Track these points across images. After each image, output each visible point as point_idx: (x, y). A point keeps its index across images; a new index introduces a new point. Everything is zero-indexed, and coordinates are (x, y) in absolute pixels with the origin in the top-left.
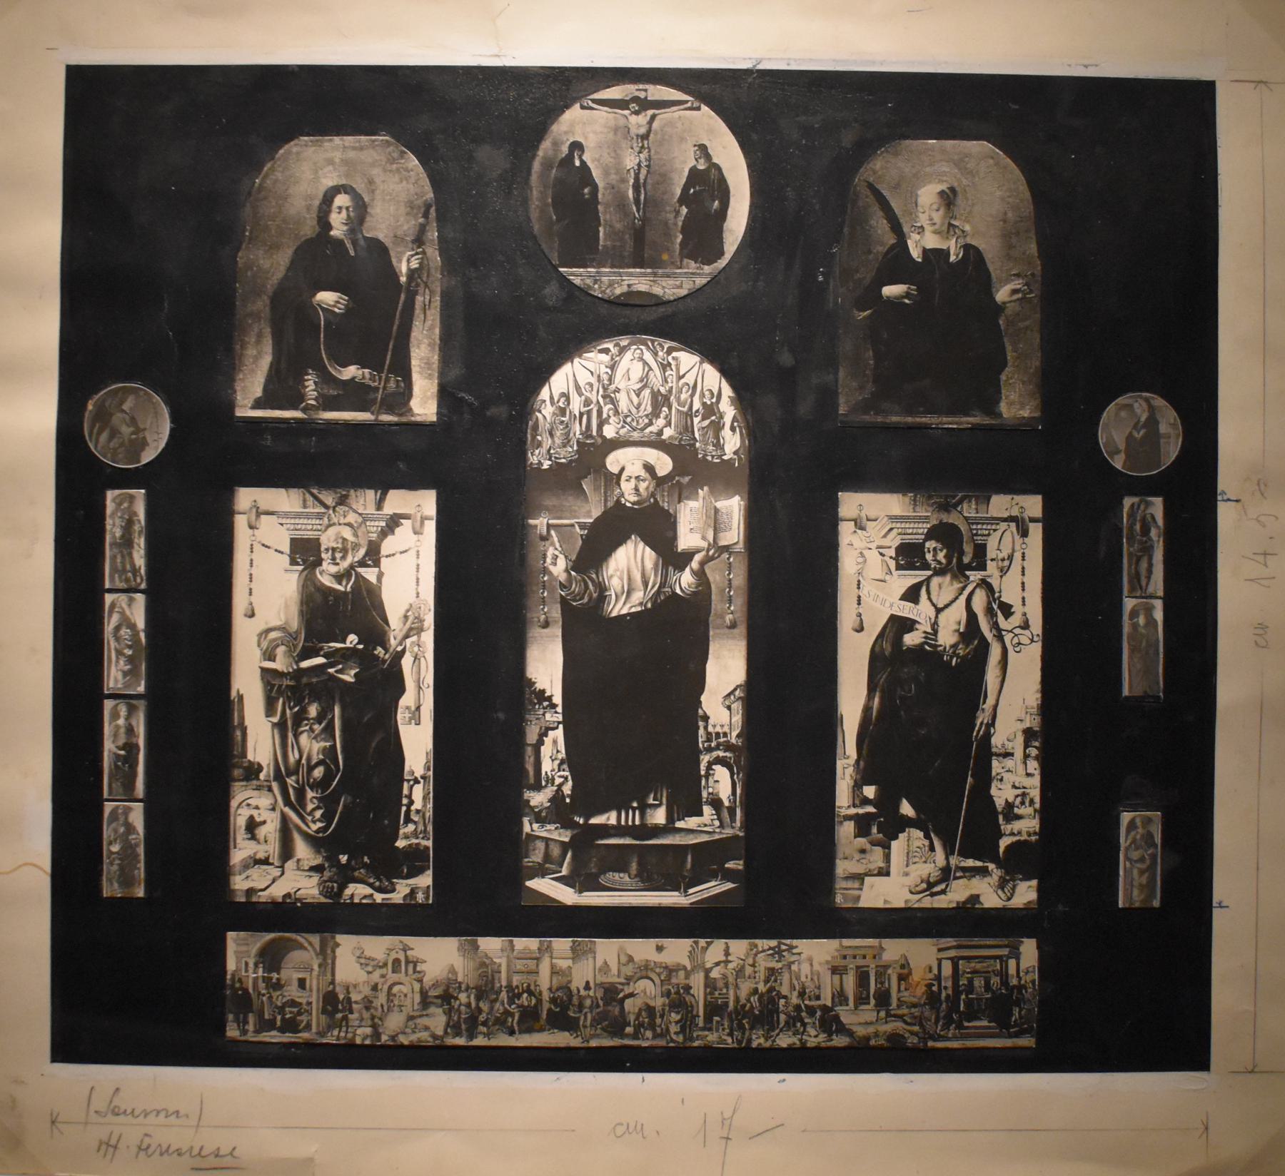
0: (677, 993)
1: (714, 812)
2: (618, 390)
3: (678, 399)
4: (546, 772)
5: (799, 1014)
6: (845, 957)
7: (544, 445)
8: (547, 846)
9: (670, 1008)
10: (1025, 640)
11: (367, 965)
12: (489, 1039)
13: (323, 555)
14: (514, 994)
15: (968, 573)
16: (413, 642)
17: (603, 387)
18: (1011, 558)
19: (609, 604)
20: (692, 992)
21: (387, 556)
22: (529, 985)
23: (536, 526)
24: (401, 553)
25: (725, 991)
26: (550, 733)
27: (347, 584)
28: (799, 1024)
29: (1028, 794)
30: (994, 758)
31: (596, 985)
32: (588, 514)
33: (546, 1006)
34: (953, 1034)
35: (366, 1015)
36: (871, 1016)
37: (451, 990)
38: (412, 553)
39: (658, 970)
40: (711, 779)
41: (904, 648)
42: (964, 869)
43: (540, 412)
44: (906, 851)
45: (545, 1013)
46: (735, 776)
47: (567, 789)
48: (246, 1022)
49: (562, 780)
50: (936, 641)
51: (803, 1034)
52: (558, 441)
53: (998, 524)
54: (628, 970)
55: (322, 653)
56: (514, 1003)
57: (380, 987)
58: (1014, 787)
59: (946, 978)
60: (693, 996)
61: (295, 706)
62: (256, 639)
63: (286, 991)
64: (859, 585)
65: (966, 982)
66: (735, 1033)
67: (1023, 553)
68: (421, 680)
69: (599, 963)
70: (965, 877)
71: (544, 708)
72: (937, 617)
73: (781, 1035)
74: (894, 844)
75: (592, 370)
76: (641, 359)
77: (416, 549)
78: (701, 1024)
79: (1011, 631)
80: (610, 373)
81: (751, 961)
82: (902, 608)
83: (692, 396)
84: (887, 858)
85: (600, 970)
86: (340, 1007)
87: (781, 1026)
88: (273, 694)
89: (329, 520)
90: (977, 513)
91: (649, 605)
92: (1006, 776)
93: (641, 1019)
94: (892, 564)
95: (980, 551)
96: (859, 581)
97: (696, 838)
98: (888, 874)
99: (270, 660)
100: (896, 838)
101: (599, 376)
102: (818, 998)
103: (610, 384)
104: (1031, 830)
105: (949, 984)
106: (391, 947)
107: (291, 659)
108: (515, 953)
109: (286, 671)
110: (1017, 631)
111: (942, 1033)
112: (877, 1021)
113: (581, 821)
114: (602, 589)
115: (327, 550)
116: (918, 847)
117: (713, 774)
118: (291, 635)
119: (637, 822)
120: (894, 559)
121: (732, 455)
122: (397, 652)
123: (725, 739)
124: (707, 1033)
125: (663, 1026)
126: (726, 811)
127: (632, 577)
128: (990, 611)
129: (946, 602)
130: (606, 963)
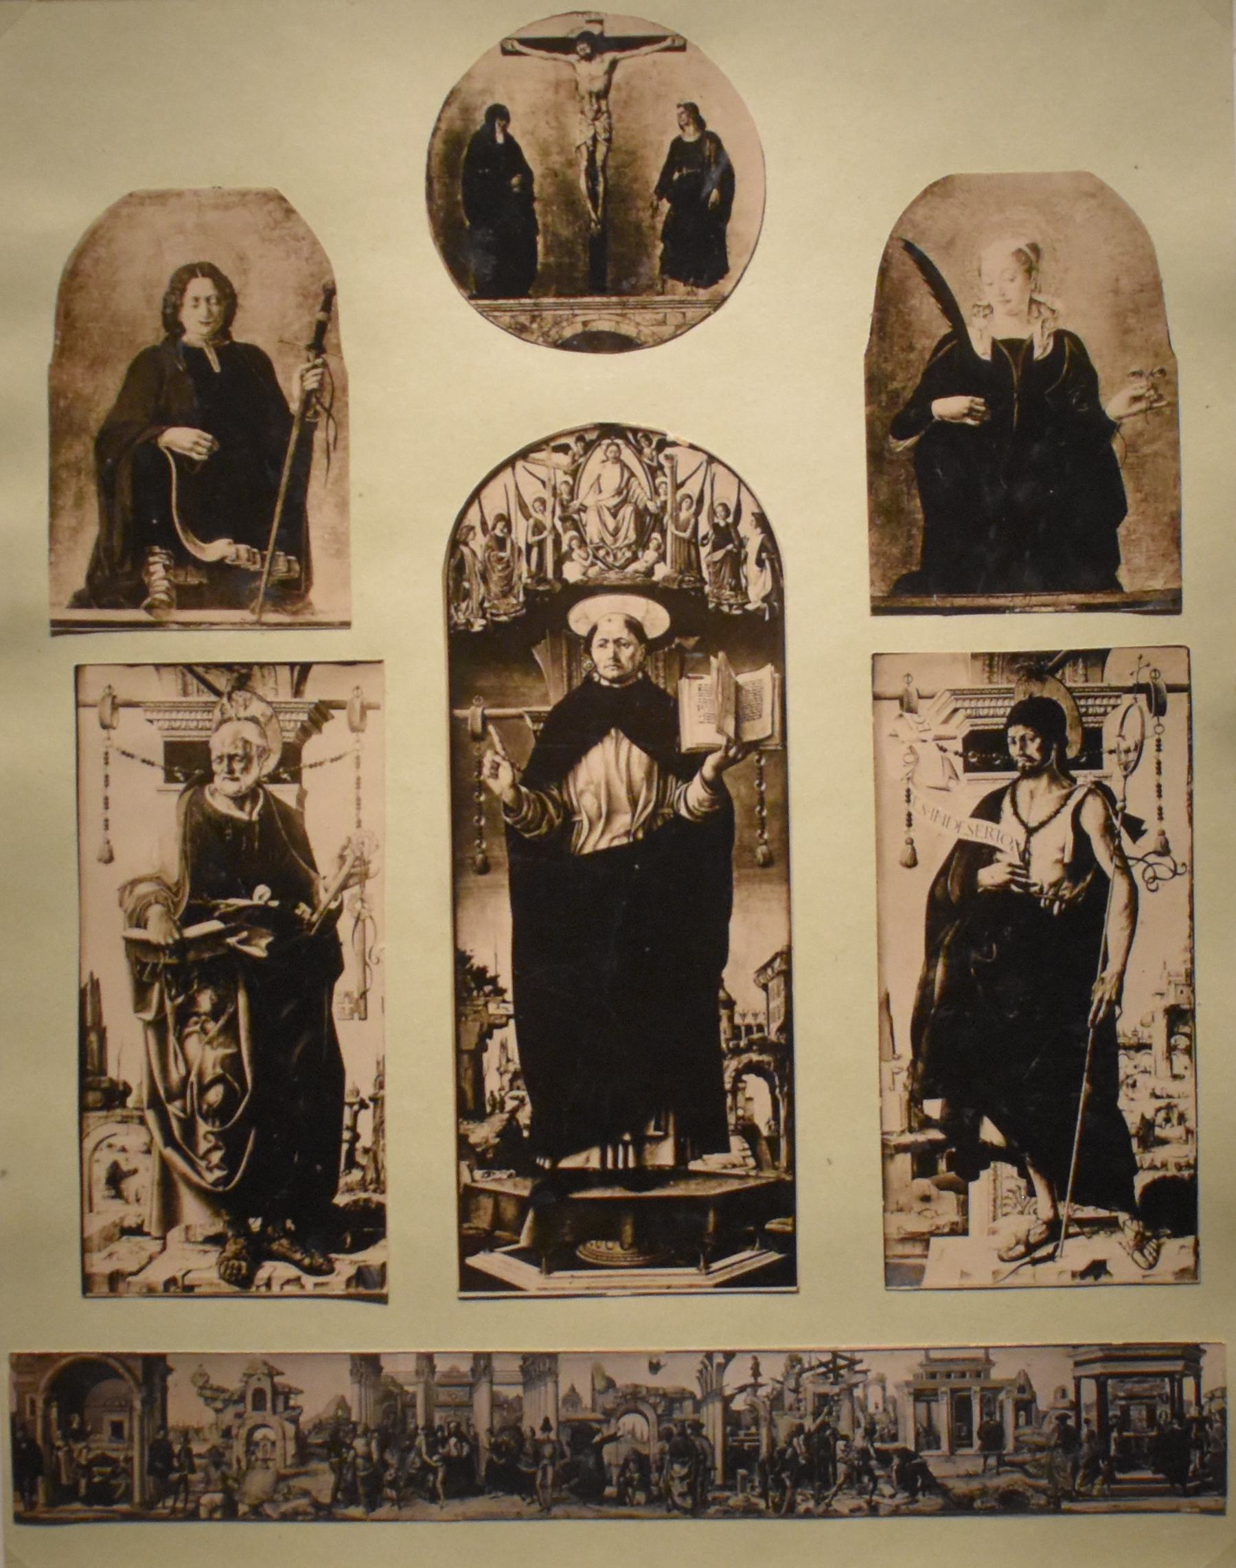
0: (682, 1433)
1: (746, 1146)
2: (583, 509)
3: (676, 519)
4: (492, 1093)
5: (866, 1463)
6: (933, 1376)
7: (474, 595)
8: (496, 1206)
9: (672, 1455)
10: (1163, 872)
11: (214, 1399)
12: (400, 1508)
13: (216, 767)
14: (435, 1439)
15: (1074, 773)
16: (353, 896)
17: (562, 506)
18: (1139, 748)
19: (579, 835)
20: (704, 1432)
21: (311, 766)
22: (458, 1425)
23: (466, 719)
24: (332, 760)
25: (753, 1430)
26: (496, 1032)
27: (252, 809)
28: (866, 1479)
29: (1176, 1106)
30: (1121, 1052)
31: (559, 1423)
32: (544, 699)
33: (485, 1456)
34: (1099, 1491)
35: (215, 1474)
36: (976, 1465)
37: (341, 1434)
38: (349, 761)
39: (652, 1400)
40: (740, 1097)
41: (980, 890)
42: (1081, 1223)
43: (466, 544)
44: (992, 1197)
45: (483, 1467)
46: (777, 1091)
47: (524, 1117)
48: (34, 1491)
49: (516, 1103)
50: (1027, 877)
51: (872, 1493)
52: (495, 589)
53: (1118, 697)
54: (608, 1401)
55: (217, 914)
56: (436, 1453)
57: (234, 1432)
58: (1155, 1096)
59: (1088, 1407)
60: (706, 1438)
61: (178, 995)
62: (116, 895)
63: (95, 1441)
64: (908, 796)
65: (1118, 1413)
66: (771, 1493)
67: (1159, 741)
68: (367, 950)
69: (563, 1390)
70: (1082, 1234)
71: (487, 995)
72: (1028, 842)
73: (840, 1496)
74: (973, 1187)
75: (546, 479)
76: (618, 460)
77: (355, 754)
78: (719, 1481)
79: (1142, 860)
80: (571, 482)
81: (792, 1383)
82: (974, 828)
83: (697, 513)
84: (964, 1207)
85: (565, 1401)
86: (176, 1463)
87: (840, 1481)
88: (145, 979)
89: (223, 714)
90: (1087, 681)
91: (640, 835)
92: (1141, 1079)
93: (628, 1475)
94: (959, 763)
95: (1093, 739)
96: (908, 791)
97: (720, 1185)
98: (965, 1232)
99: (138, 925)
100: (975, 1177)
101: (554, 488)
102: (894, 1438)
103: (572, 500)
104: (1183, 1161)
105: (1093, 1415)
106: (250, 1372)
107: (171, 924)
108: (437, 1378)
109: (163, 943)
110: (1152, 859)
111: (1082, 1489)
112: (984, 1471)
113: (547, 1165)
114: (568, 812)
115: (221, 758)
116: (1010, 1191)
117: (744, 1089)
118: (169, 888)
119: (631, 1164)
120: (961, 755)
121: (759, 604)
122: (330, 911)
123: (760, 1035)
124: (727, 1494)
125: (661, 1484)
126: (764, 1143)
127: (613, 792)
128: (1109, 831)
129: (1043, 817)
130: (573, 1389)
